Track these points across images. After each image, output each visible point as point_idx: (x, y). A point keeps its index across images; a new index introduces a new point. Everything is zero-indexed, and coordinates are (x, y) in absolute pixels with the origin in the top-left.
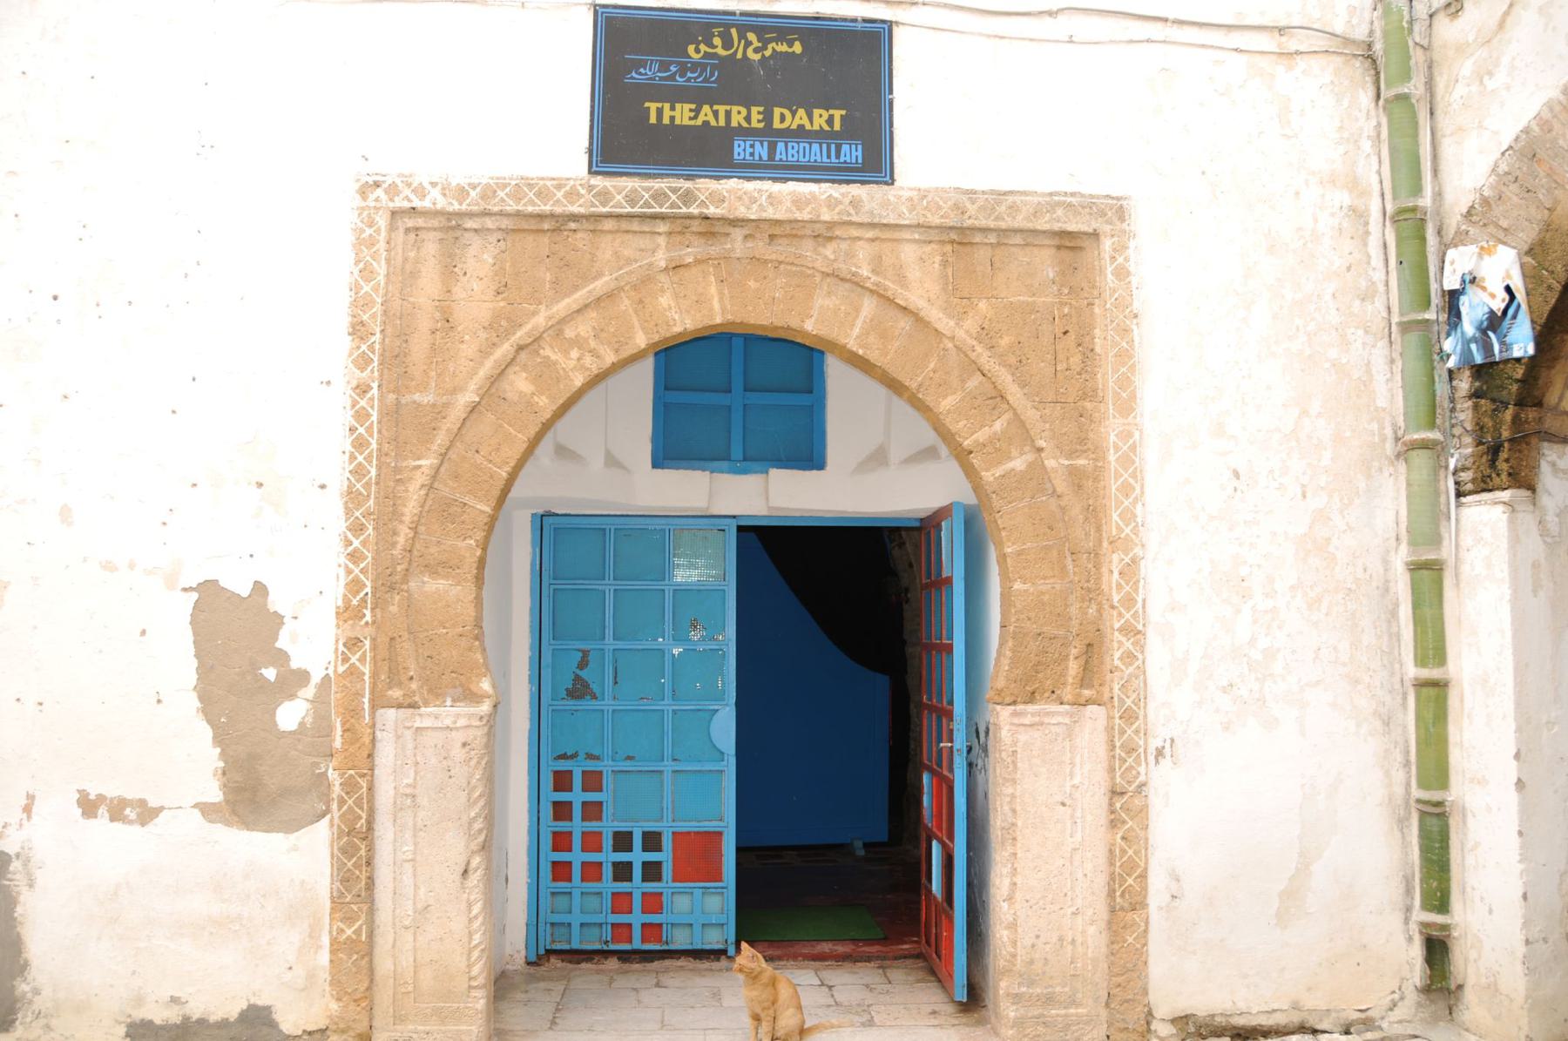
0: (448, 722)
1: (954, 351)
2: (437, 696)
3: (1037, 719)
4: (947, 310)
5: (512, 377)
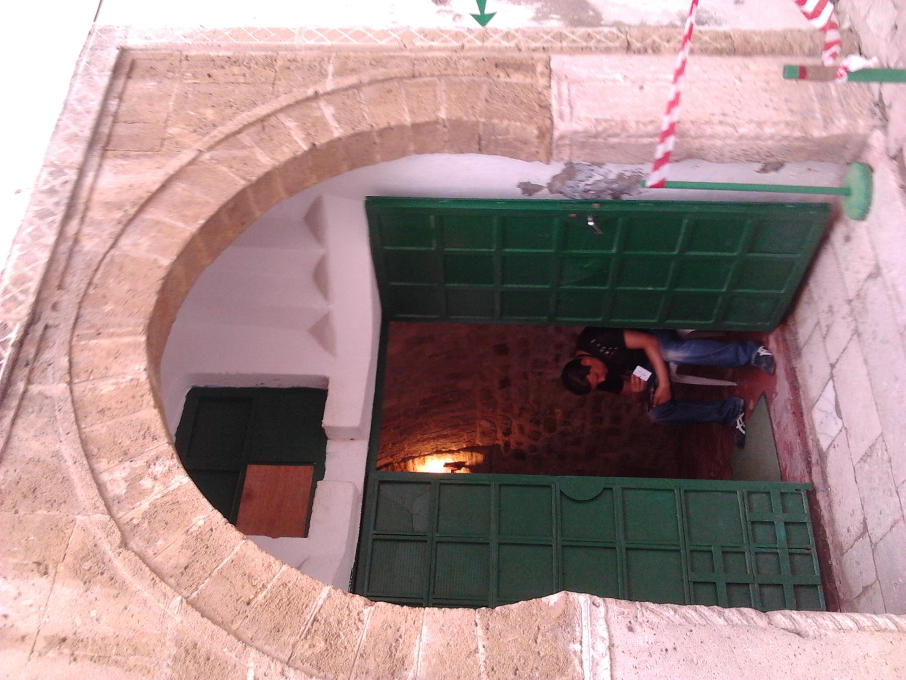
0: (602, 647)
1: (214, 153)
2: (568, 661)
3: (565, 103)
4: (171, 155)
5: (159, 559)
